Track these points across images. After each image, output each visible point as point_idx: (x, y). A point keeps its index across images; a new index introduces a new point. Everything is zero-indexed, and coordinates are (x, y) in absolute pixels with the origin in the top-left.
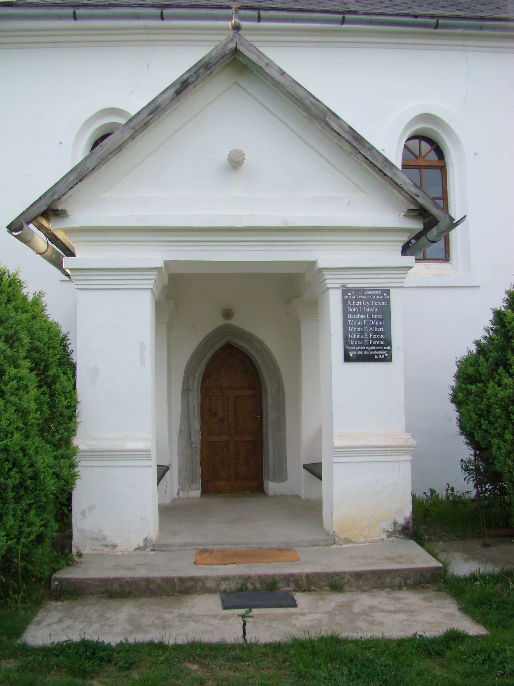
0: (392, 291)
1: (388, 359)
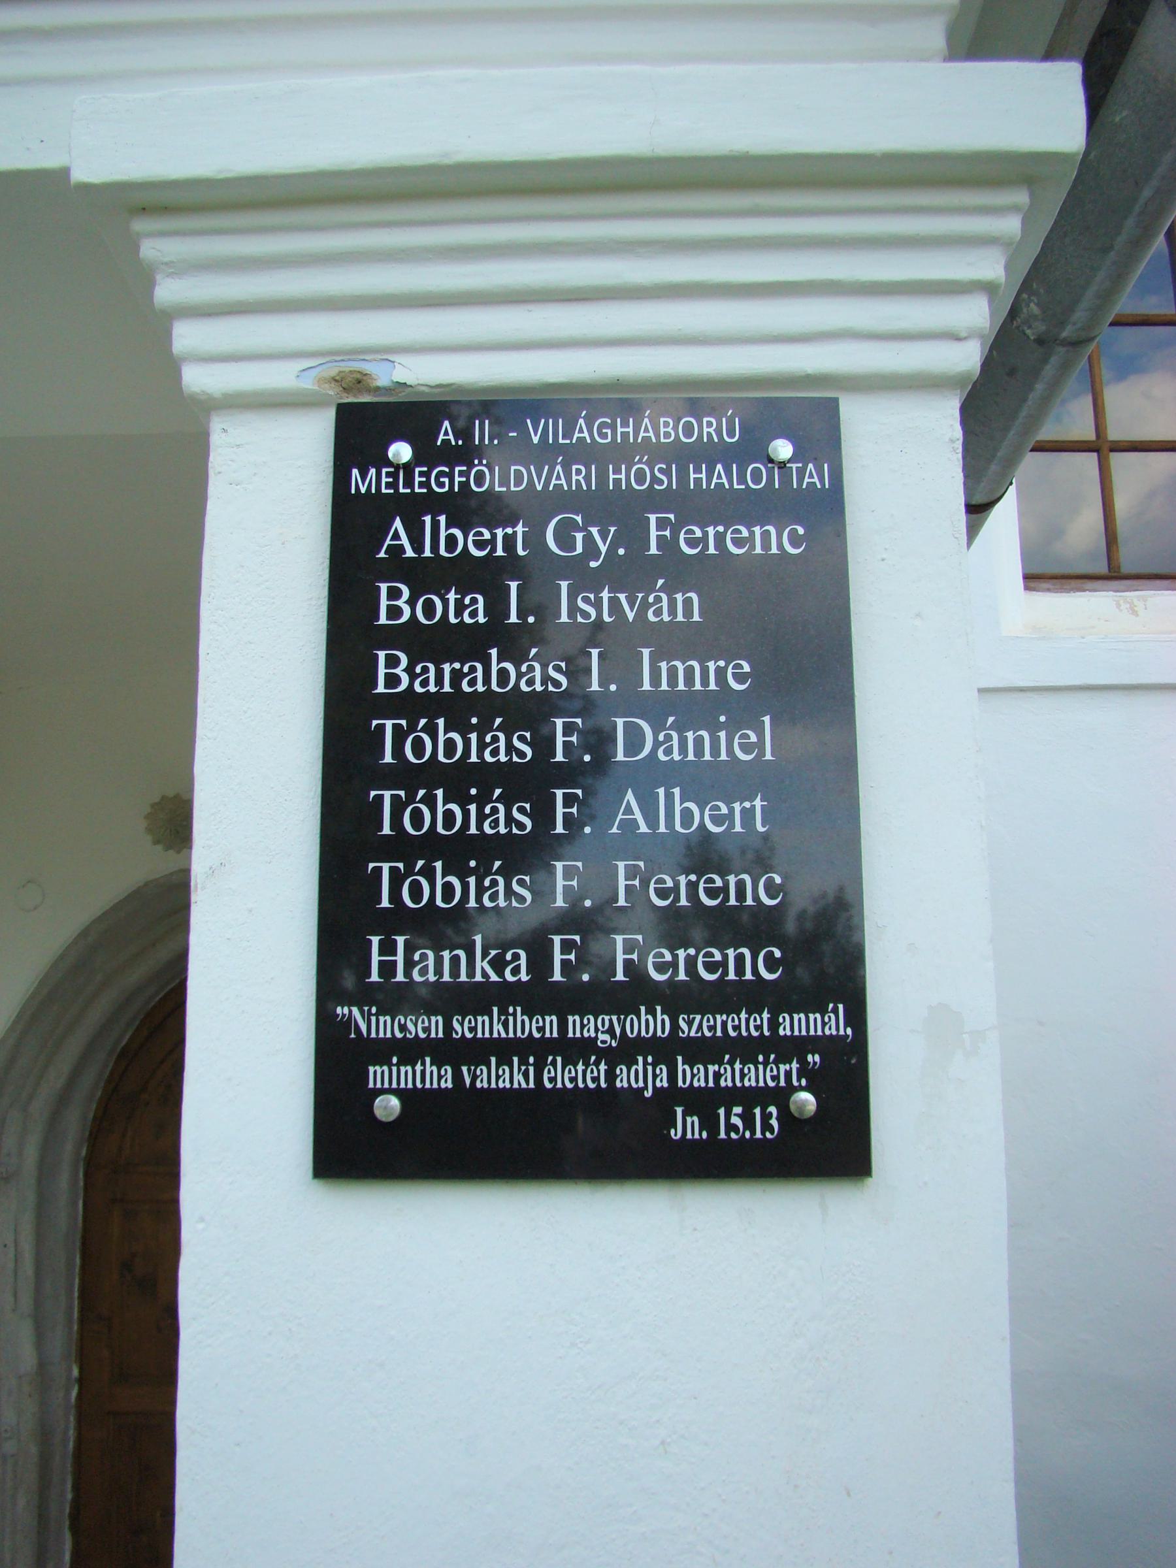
0: (860, 421)
1: (829, 1142)
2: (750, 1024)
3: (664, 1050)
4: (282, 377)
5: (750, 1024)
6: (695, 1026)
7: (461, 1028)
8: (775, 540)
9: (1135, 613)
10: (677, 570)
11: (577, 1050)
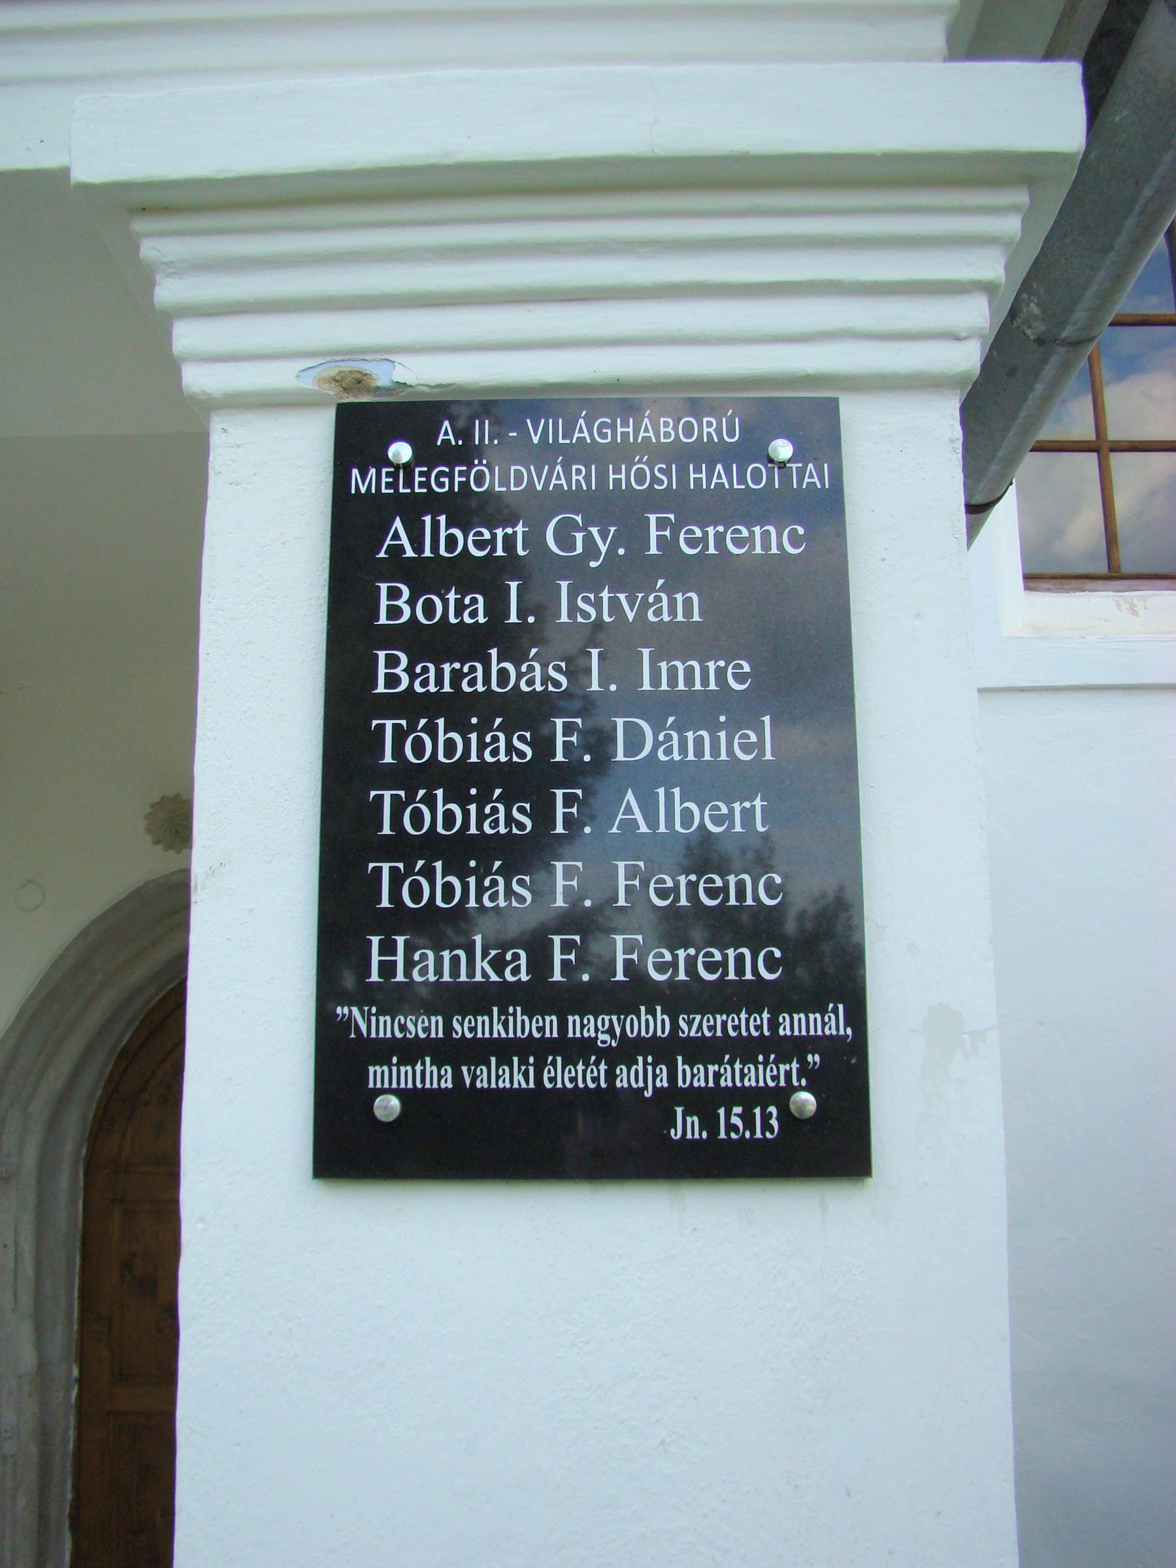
1: (829, 1142)
2: (750, 1024)
3: (664, 1050)
4: (282, 377)
5: (750, 1024)
6: (695, 1026)
7: (461, 1028)
8: (775, 540)
9: (1135, 613)
10: (677, 570)
11: (577, 1050)
